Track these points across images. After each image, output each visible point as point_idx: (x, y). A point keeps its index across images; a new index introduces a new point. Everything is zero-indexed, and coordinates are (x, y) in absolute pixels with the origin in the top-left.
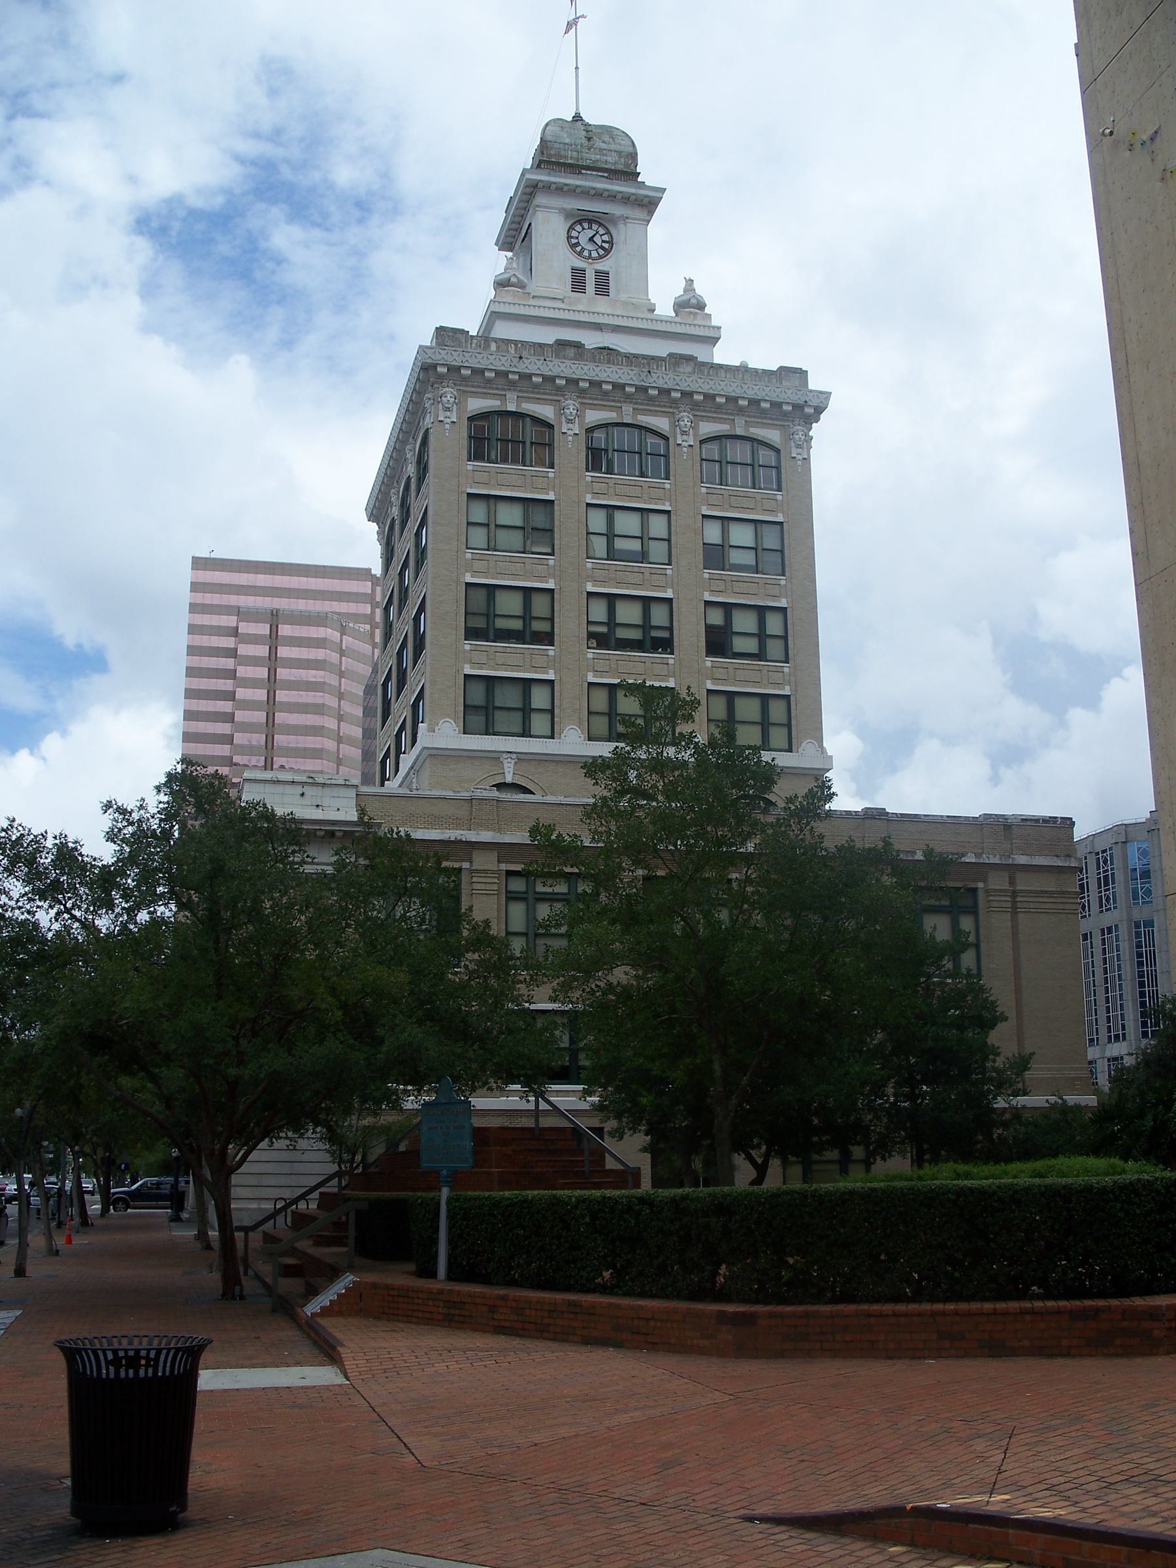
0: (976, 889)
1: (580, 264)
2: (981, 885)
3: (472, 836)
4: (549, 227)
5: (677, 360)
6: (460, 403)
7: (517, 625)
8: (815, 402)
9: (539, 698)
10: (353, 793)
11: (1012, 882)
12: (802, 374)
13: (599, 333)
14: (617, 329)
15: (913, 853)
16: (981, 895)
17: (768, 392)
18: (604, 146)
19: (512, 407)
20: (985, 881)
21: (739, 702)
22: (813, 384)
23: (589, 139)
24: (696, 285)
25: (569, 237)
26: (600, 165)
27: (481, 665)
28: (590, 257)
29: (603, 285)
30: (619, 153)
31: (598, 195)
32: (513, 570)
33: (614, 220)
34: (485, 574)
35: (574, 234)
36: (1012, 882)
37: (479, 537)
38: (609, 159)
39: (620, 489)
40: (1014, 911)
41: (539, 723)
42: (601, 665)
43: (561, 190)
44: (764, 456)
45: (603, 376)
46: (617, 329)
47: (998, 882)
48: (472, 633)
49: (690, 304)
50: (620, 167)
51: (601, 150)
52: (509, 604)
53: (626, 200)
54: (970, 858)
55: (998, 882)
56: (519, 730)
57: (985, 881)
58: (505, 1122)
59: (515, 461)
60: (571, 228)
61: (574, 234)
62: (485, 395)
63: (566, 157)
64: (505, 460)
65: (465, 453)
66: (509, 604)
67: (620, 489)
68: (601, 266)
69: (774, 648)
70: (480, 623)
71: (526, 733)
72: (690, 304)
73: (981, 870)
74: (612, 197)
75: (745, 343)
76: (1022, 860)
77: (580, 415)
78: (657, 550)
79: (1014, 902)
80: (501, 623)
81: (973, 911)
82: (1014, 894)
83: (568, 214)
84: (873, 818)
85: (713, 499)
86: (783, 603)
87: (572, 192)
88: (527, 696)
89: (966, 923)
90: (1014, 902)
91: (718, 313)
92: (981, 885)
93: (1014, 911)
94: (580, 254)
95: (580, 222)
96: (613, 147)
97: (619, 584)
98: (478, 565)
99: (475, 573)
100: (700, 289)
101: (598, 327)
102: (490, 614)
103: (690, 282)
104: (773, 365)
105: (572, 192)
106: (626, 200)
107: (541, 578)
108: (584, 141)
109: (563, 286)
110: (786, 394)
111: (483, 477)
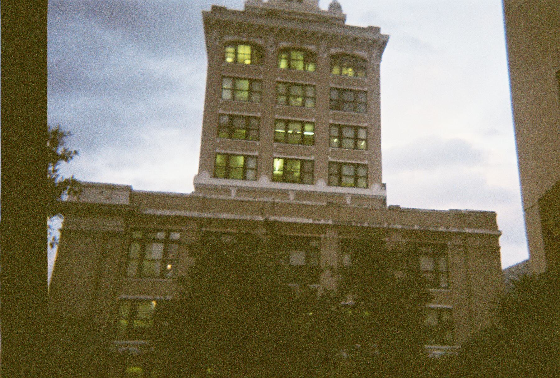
2: (449, 243)
3: (187, 214)
6: (328, 48)
8: (383, 39)
12: (378, 29)
15: (413, 226)
41: (362, 182)
49: (335, 7)
56: (365, 186)
62: (286, 41)
72: (335, 7)
76: (469, 230)
77: (276, 44)
81: (445, 255)
82: (465, 247)
84: (393, 210)
88: (356, 171)
91: (345, 10)
104: (365, 25)
110: (373, 36)
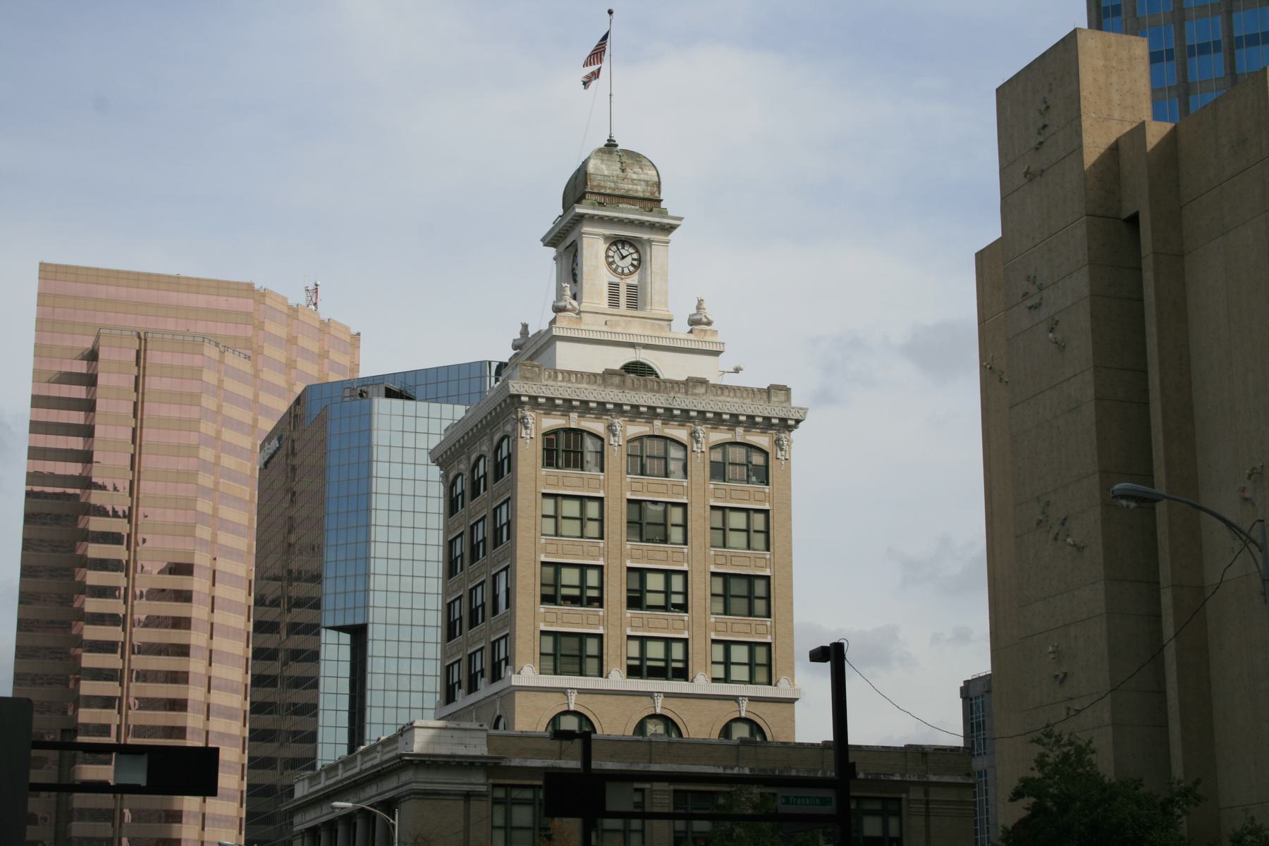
0: (900, 799)
1: (615, 280)
2: (904, 796)
4: (594, 247)
5: (693, 383)
7: (576, 592)
8: (797, 416)
9: (592, 647)
10: (484, 735)
11: (926, 793)
12: (786, 390)
13: (632, 350)
14: (647, 346)
16: (904, 803)
17: (760, 409)
18: (635, 176)
19: (573, 426)
20: (907, 792)
21: (734, 648)
22: (796, 401)
23: (623, 171)
24: (705, 305)
25: (607, 257)
26: (632, 194)
27: (552, 623)
28: (623, 273)
29: (636, 298)
30: (647, 182)
31: (631, 223)
32: (573, 551)
33: (639, 240)
34: (556, 554)
35: (611, 253)
36: (926, 793)
37: (549, 525)
38: (639, 188)
39: (652, 488)
40: (927, 815)
41: (592, 665)
42: (637, 622)
43: (602, 220)
44: (757, 459)
45: (641, 402)
46: (647, 346)
47: (916, 794)
48: (546, 599)
50: (647, 195)
51: (633, 180)
52: (570, 577)
53: (652, 226)
54: (897, 777)
55: (916, 794)
57: (907, 792)
58: (100, 756)
59: (575, 466)
60: (609, 249)
61: (611, 253)
63: (605, 187)
64: (567, 466)
65: (540, 461)
66: (570, 577)
67: (652, 488)
68: (634, 280)
69: (760, 606)
70: (550, 591)
71: (581, 673)
73: (904, 785)
74: (642, 225)
75: (748, 359)
76: (933, 778)
78: (676, 534)
79: (927, 809)
80: (565, 591)
81: (898, 814)
82: (927, 803)
83: (606, 238)
85: (719, 493)
86: (767, 572)
87: (610, 221)
89: (893, 823)
90: (927, 809)
91: (723, 329)
92: (904, 796)
93: (927, 815)
94: (615, 271)
95: (615, 243)
96: (642, 177)
97: (650, 560)
98: (550, 548)
99: (547, 554)
100: (710, 312)
101: (632, 345)
102: (556, 584)
103: (700, 302)
105: (610, 221)
106: (652, 226)
107: (594, 557)
108: (619, 172)
109: (604, 304)
110: (774, 410)
111: (554, 480)
